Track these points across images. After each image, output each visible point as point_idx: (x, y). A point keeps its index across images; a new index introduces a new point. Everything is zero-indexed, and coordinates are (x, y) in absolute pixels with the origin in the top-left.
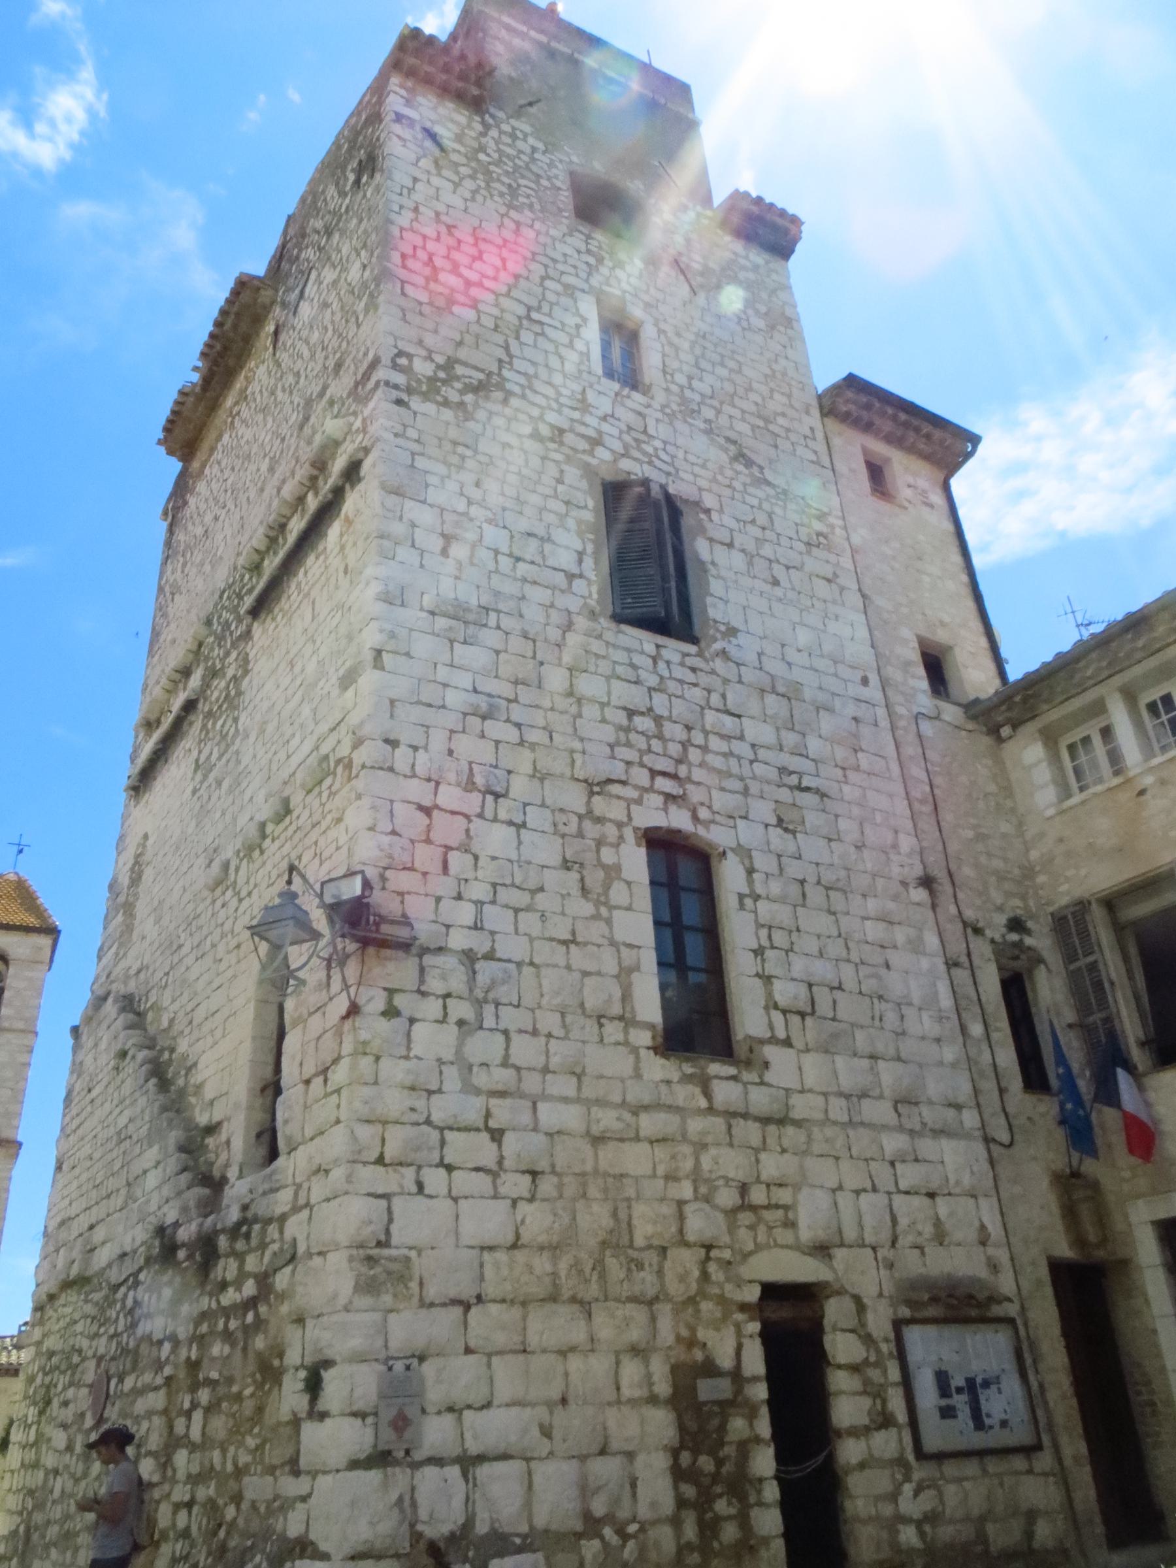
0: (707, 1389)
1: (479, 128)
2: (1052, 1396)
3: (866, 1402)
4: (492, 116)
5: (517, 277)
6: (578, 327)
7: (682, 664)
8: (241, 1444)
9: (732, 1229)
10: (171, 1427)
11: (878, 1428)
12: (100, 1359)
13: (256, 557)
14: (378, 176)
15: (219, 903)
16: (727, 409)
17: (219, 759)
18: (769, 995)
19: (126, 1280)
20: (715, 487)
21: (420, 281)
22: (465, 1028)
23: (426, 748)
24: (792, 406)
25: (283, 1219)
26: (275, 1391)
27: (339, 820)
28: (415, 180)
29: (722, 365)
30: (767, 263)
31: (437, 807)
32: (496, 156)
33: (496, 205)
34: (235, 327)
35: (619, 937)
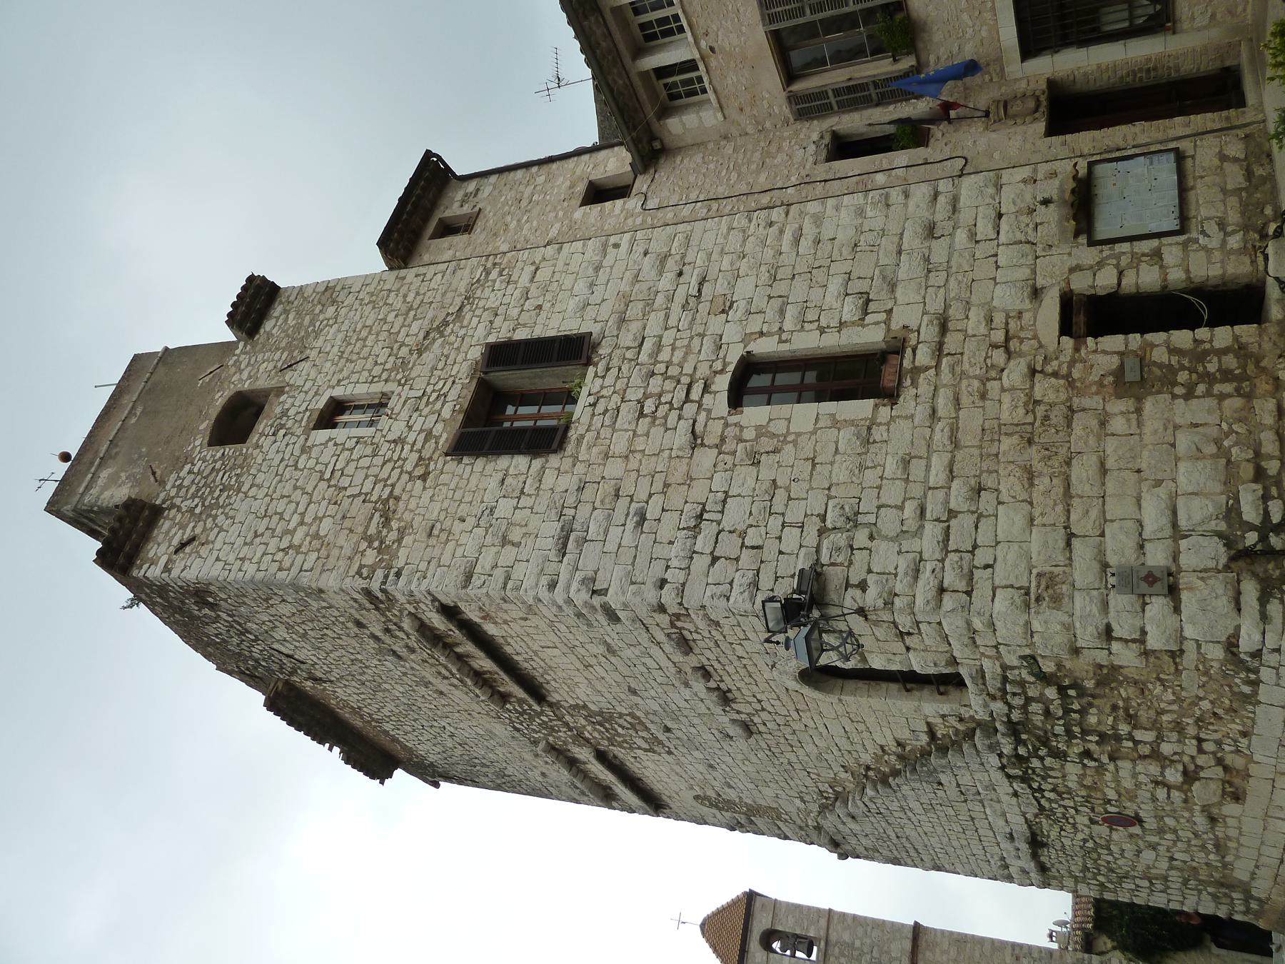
0: (1131, 375)
1: (173, 511)
2: (1142, 139)
3: (1143, 266)
4: (164, 502)
5: (295, 488)
7: (603, 377)
8: (1159, 699)
9: (1020, 354)
10: (1145, 757)
11: (1162, 259)
12: (1092, 821)
14: (212, 588)
15: (762, 728)
17: (647, 729)
18: (853, 323)
19: (1035, 798)
20: (464, 349)
21: (300, 558)
22: (875, 535)
23: (668, 560)
24: (398, 290)
25: (1005, 668)
26: (1124, 671)
27: (717, 624)
28: (218, 559)
29: (365, 340)
30: (281, 303)
31: (712, 553)
32: (197, 500)
33: (236, 500)
35: (811, 428)
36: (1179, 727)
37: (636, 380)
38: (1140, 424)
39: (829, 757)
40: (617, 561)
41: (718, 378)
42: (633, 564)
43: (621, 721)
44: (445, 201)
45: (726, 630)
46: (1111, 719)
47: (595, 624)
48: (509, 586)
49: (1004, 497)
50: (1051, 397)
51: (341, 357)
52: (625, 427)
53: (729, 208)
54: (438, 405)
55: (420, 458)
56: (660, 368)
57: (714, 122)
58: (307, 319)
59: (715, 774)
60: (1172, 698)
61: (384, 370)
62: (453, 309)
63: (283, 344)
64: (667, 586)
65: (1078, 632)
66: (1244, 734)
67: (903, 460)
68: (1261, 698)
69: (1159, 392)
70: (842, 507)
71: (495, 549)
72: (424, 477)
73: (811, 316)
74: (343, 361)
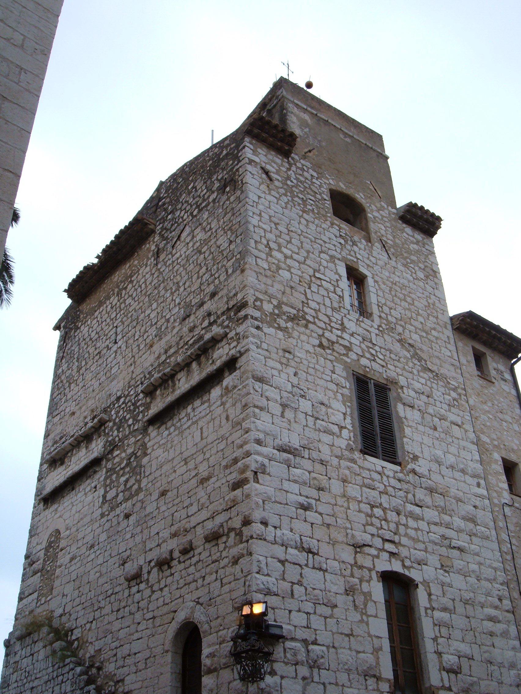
1: (287, 165)
4: (293, 159)
5: (308, 252)
7: (394, 478)
14: (239, 192)
15: (134, 589)
17: (126, 500)
18: (441, 663)
20: (405, 374)
21: (264, 256)
22: (306, 681)
24: (438, 324)
28: (259, 197)
30: (423, 239)
31: (287, 560)
32: (295, 181)
33: (297, 210)
35: (373, 632)
37: (396, 502)
40: (274, 490)
41: (399, 563)
42: (276, 502)
43: (132, 481)
44: (497, 357)
45: (229, 570)
47: (228, 471)
48: (257, 411)
51: (392, 282)
52: (364, 495)
53: (509, 568)
54: (367, 355)
55: (333, 343)
56: (403, 520)
58: (414, 258)
59: (84, 549)
61: (386, 314)
62: (430, 365)
63: (397, 241)
64: (263, 527)
70: (322, 657)
71: (278, 398)
72: (321, 345)
73: (444, 631)
74: (390, 284)
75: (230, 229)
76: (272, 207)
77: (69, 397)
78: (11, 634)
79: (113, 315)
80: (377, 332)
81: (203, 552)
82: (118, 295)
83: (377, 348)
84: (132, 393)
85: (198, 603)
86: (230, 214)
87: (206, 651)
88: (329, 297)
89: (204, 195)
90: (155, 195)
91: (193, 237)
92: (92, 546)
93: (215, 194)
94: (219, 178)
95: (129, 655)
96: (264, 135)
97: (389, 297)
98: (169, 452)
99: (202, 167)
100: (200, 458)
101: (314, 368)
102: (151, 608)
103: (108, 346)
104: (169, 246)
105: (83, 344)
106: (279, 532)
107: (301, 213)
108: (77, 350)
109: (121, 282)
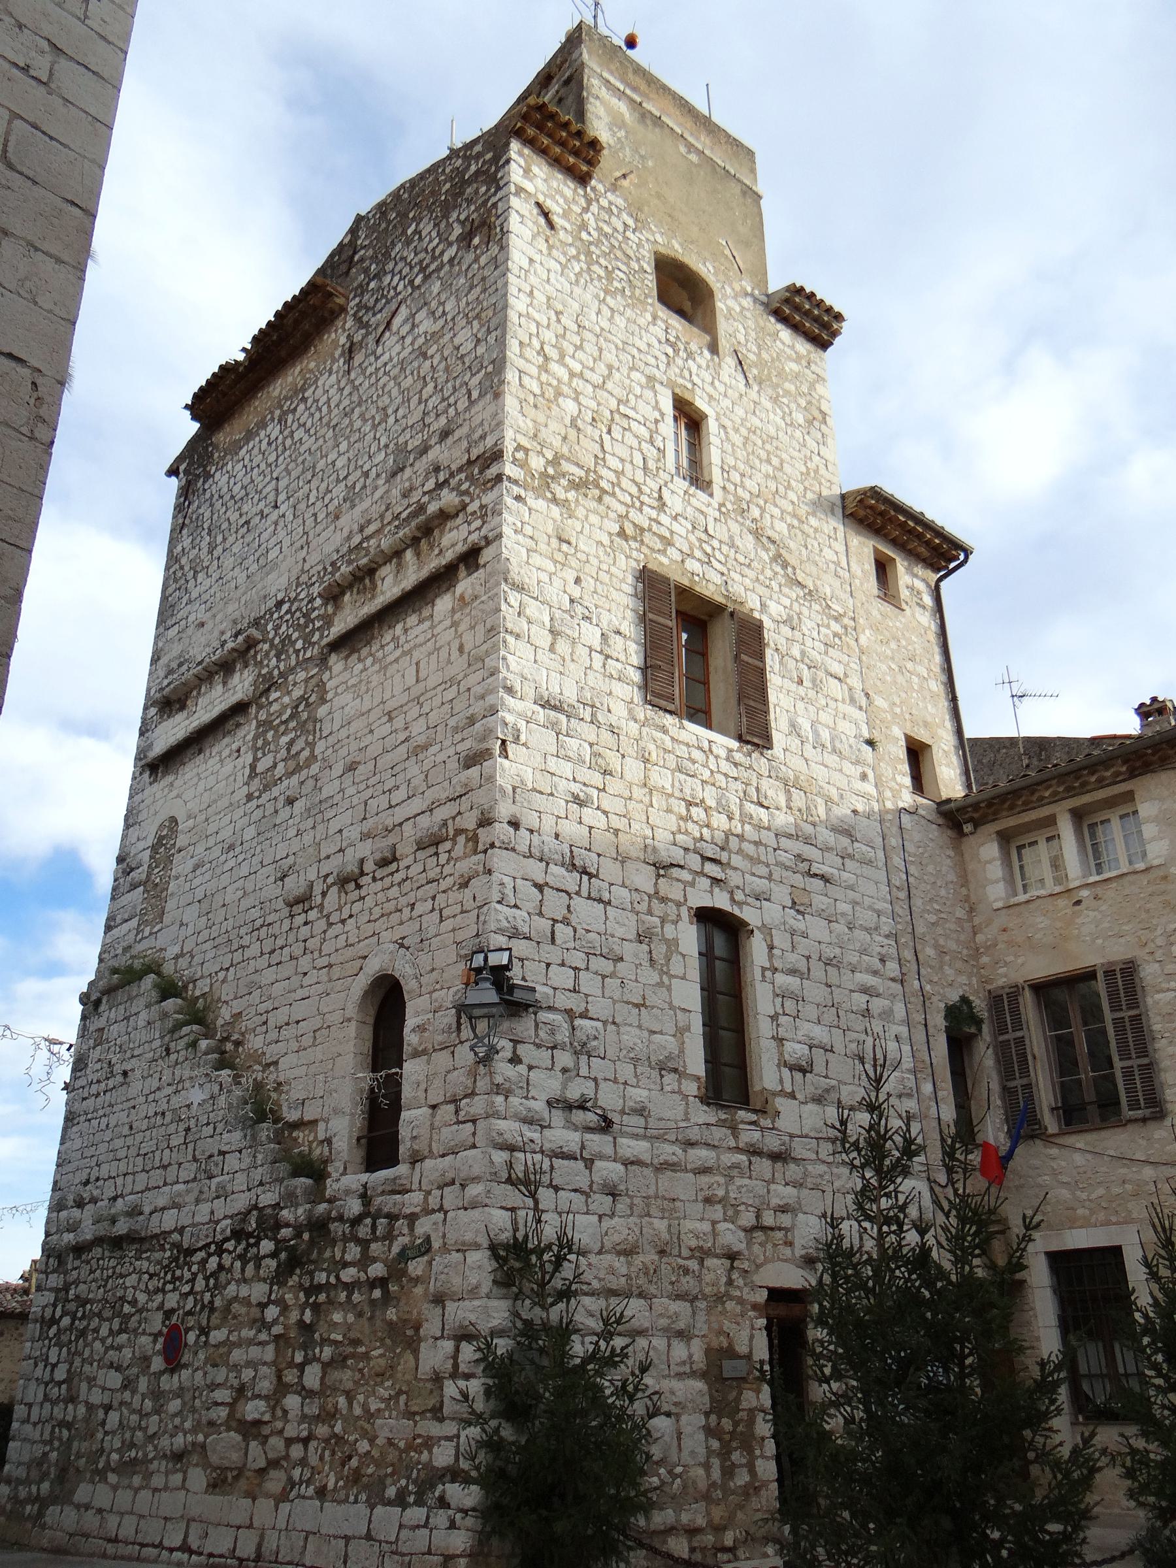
1: (583, 202)
4: (594, 189)
5: (610, 367)
6: (657, 421)
7: (727, 759)
9: (749, 1243)
12: (168, 1314)
13: (336, 590)
14: (494, 249)
16: (770, 508)
17: (289, 774)
18: (781, 1054)
19: (208, 1245)
21: (534, 371)
25: (412, 1218)
27: (465, 885)
28: (531, 260)
29: (769, 462)
30: (809, 352)
32: (595, 234)
34: (297, 322)
35: (676, 1003)
36: (328, 1416)
38: (680, 1376)
39: (256, 996)
43: (300, 744)
45: (454, 896)
46: (340, 1338)
47: (458, 737)
49: (607, 1223)
50: (708, 1277)
51: (749, 430)
52: (677, 784)
55: (642, 530)
57: (992, 898)
58: (789, 386)
59: (217, 852)
60: (373, 1408)
64: (511, 830)
65: (467, 1303)
66: (321, 1493)
67: (644, 1109)
68: (379, 1510)
69: (711, 1397)
70: (596, 1038)
71: (547, 620)
73: (790, 1005)
75: (478, 316)
76: (552, 280)
77: (194, 595)
78: (91, 984)
79: (272, 458)
80: (717, 514)
81: (413, 865)
82: (280, 422)
83: (716, 544)
84: (302, 596)
85: (402, 946)
86: (479, 289)
87: (410, 1022)
88: (640, 450)
89: (434, 249)
90: (346, 241)
91: (414, 326)
92: (231, 847)
93: (455, 248)
94: (462, 217)
95: (287, 1024)
96: (546, 141)
97: (741, 454)
98: (357, 694)
99: (433, 193)
100: (414, 712)
101: (608, 572)
102: (326, 949)
103: (262, 512)
104: (371, 340)
105: (218, 505)
106: (535, 838)
107: (602, 295)
108: (207, 514)
109: (286, 398)
